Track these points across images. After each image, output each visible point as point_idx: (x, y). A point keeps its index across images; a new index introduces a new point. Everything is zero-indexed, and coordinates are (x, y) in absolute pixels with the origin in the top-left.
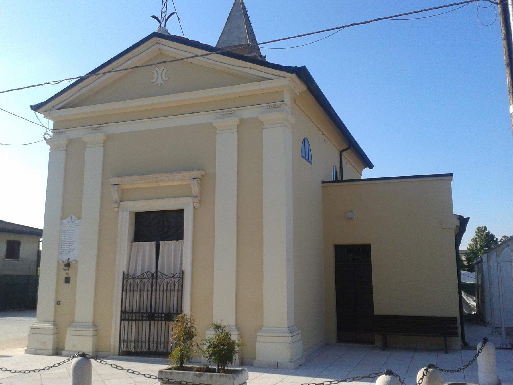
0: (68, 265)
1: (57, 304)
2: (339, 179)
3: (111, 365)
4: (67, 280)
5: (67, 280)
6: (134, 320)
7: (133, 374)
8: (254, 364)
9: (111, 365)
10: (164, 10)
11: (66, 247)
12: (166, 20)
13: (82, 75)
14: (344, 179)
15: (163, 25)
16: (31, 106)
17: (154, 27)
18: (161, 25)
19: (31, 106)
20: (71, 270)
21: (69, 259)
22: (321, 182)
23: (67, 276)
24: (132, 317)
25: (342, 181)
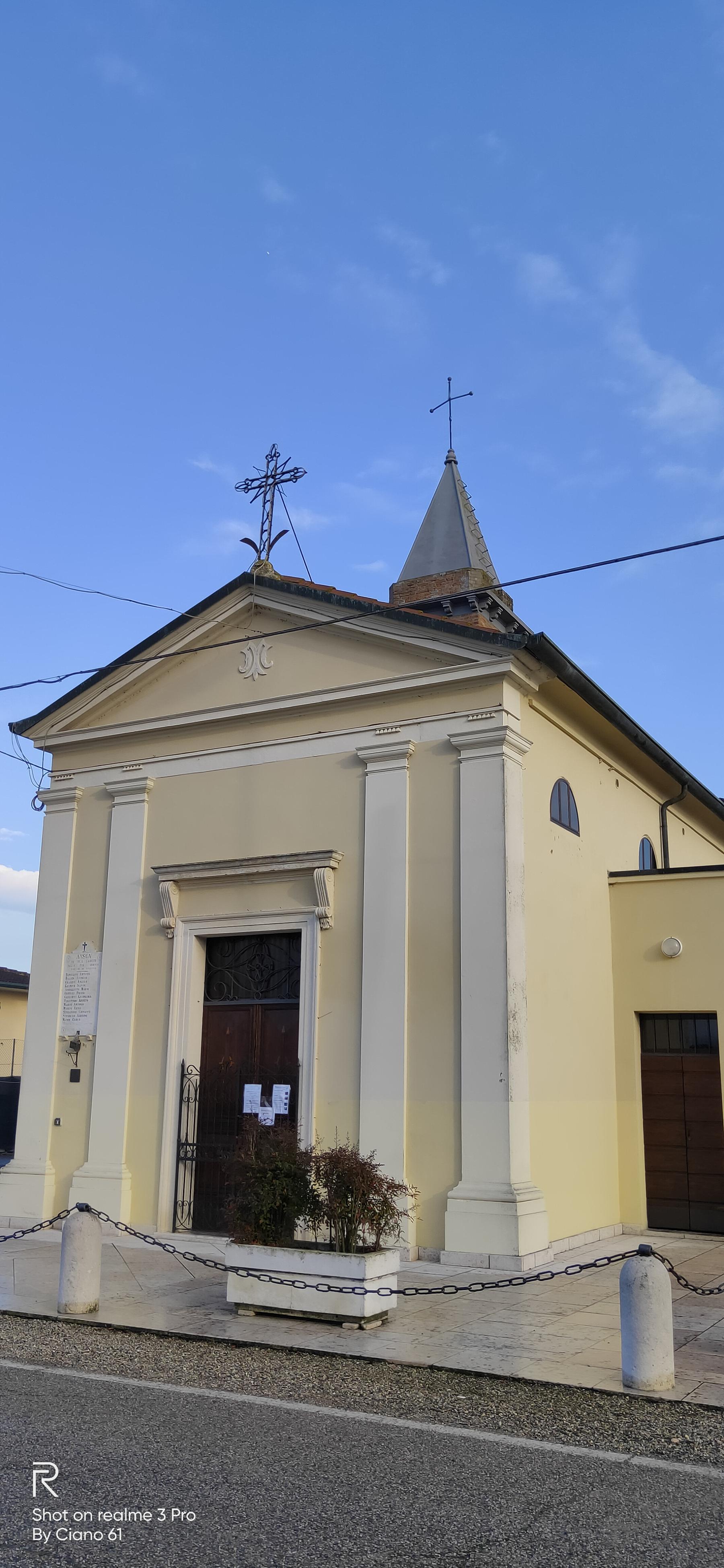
0: (75, 1046)
1: (55, 1124)
2: (659, 866)
3: (566, 1272)
4: (75, 1076)
5: (75, 1076)
6: (189, 1159)
7: (341, 1287)
8: (442, 1258)
9: (566, 1272)
10: (266, 527)
11: (73, 1007)
12: (271, 546)
13: (104, 664)
14: (672, 865)
15: (263, 556)
16: (10, 725)
17: (244, 562)
18: (259, 557)
19: (10, 725)
20: (84, 1052)
21: (78, 1032)
22: (606, 880)
23: (74, 1068)
24: (186, 1152)
25: (667, 870)
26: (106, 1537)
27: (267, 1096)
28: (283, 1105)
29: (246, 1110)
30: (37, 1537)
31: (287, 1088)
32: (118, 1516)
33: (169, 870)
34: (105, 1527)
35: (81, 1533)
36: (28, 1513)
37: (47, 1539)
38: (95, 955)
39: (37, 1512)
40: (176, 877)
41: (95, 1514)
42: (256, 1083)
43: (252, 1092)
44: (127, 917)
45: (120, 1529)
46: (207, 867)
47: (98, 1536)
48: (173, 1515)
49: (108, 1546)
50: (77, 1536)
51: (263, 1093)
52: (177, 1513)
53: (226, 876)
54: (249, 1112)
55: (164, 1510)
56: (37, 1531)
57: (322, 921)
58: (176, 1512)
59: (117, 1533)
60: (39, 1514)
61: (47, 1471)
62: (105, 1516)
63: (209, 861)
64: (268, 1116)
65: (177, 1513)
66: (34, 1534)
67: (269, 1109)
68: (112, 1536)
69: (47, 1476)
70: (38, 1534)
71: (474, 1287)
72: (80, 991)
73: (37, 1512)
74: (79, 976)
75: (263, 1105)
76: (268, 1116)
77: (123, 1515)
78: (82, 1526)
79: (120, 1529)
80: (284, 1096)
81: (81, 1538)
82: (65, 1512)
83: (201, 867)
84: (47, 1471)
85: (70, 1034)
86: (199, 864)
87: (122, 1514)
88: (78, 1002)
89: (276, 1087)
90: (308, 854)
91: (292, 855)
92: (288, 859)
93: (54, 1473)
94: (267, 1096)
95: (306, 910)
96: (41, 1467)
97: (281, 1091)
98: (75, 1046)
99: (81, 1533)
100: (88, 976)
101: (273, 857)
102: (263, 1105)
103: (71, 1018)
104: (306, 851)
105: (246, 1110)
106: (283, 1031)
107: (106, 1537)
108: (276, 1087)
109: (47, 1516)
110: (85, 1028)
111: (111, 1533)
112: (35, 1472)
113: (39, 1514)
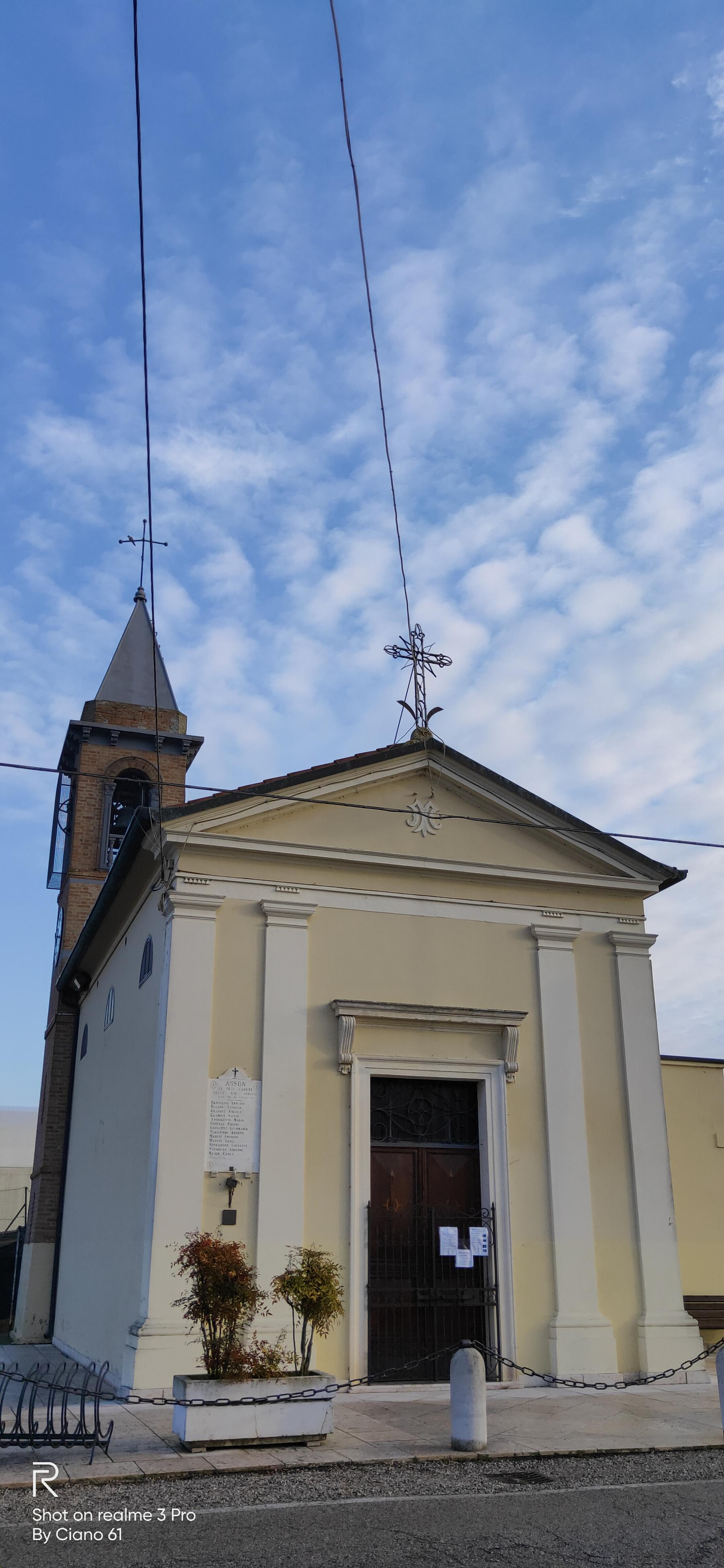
11: (223, 1139)
20: (242, 1192)
26: (106, 1536)
27: (464, 1241)
28: (481, 1247)
29: (444, 1252)
30: (37, 1537)
31: (484, 1230)
32: (118, 1516)
33: (356, 1005)
34: (106, 1526)
35: (81, 1533)
36: (30, 1517)
37: (47, 1539)
38: (252, 1084)
39: (37, 1512)
40: (360, 1013)
41: (95, 1515)
42: (451, 1226)
43: (448, 1235)
44: (291, 1048)
45: (120, 1529)
46: (398, 1008)
47: (98, 1536)
48: (173, 1516)
49: (107, 1545)
50: (78, 1536)
51: (460, 1236)
52: (176, 1513)
53: (416, 1021)
54: (446, 1254)
55: (164, 1510)
56: (37, 1531)
57: (509, 1075)
58: (176, 1512)
59: (118, 1533)
60: (40, 1515)
61: (47, 1471)
62: (107, 1516)
63: (404, 1003)
64: (464, 1260)
65: (176, 1513)
66: (34, 1534)
67: (467, 1251)
68: (112, 1536)
69: (45, 1475)
70: (38, 1534)
71: (526, 1371)
72: (233, 1122)
73: (37, 1512)
74: (230, 1105)
75: (461, 1247)
76: (464, 1260)
77: (124, 1516)
78: (82, 1526)
79: (120, 1529)
80: (482, 1238)
81: (81, 1538)
82: (65, 1513)
83: (392, 1007)
84: (47, 1471)
85: (221, 1167)
86: (391, 1004)
87: (122, 1514)
88: (230, 1134)
89: (473, 1231)
90: (505, 1012)
91: (489, 1011)
92: (484, 1014)
93: (53, 1476)
94: (464, 1241)
95: (492, 1063)
96: (41, 1467)
97: (478, 1234)
98: (231, 1184)
99: (81, 1533)
100: (242, 1106)
101: (471, 1010)
102: (461, 1247)
103: (221, 1152)
104: (503, 1009)
105: (444, 1252)
106: (451, 1175)
107: (106, 1536)
108: (473, 1231)
109: (47, 1516)
110: (243, 1164)
111: (111, 1533)
112: (35, 1472)
113: (40, 1515)
